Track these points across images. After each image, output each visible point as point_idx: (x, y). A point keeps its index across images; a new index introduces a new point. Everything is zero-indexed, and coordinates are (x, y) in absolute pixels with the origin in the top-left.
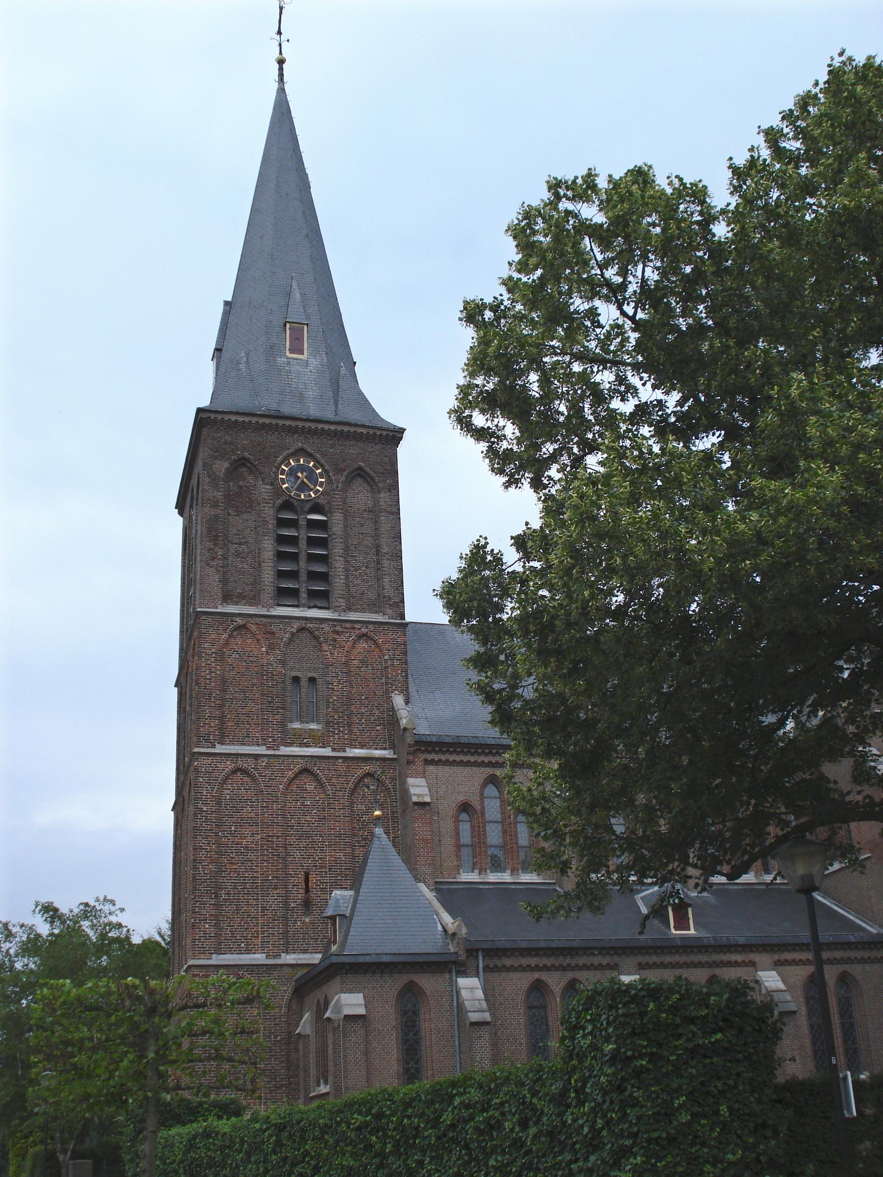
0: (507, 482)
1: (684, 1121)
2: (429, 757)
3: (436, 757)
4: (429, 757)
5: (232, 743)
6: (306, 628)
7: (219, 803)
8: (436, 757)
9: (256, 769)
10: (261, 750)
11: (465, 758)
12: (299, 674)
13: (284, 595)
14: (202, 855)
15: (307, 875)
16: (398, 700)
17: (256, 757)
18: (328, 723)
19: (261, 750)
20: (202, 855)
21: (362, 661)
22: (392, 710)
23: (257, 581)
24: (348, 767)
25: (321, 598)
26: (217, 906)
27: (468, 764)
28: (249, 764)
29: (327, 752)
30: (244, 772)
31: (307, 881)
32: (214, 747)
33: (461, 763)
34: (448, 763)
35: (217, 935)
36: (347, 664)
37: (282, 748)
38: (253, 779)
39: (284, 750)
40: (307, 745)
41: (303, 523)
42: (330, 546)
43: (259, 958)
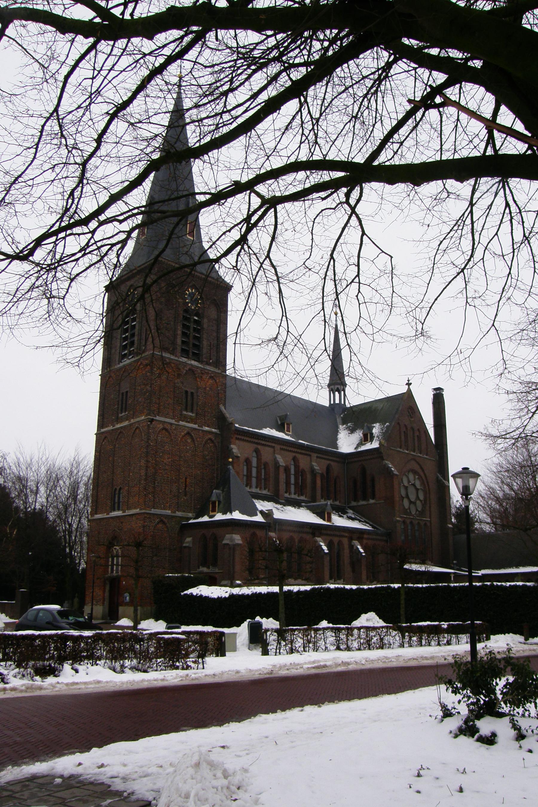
0: (500, 498)
1: (103, 644)
2: (238, 436)
3: (240, 437)
4: (238, 436)
5: (162, 416)
6: (192, 371)
7: (156, 442)
8: (240, 437)
9: (171, 429)
10: (173, 421)
11: (249, 439)
12: (188, 390)
13: (185, 353)
14: (150, 465)
15: (186, 478)
16: (222, 408)
17: (171, 424)
18: (197, 414)
19: (173, 421)
20: (150, 465)
21: (210, 388)
22: (221, 412)
23: (174, 343)
24: (204, 434)
25: (197, 357)
26: (154, 488)
27: (250, 442)
28: (168, 427)
29: (196, 426)
30: (166, 430)
31: (186, 481)
32: (156, 417)
33: (247, 441)
34: (244, 440)
35: (154, 500)
36: (205, 388)
37: (181, 422)
38: (169, 433)
39: (181, 423)
40: (189, 422)
41: (192, 320)
42: (201, 333)
43: (168, 512)
